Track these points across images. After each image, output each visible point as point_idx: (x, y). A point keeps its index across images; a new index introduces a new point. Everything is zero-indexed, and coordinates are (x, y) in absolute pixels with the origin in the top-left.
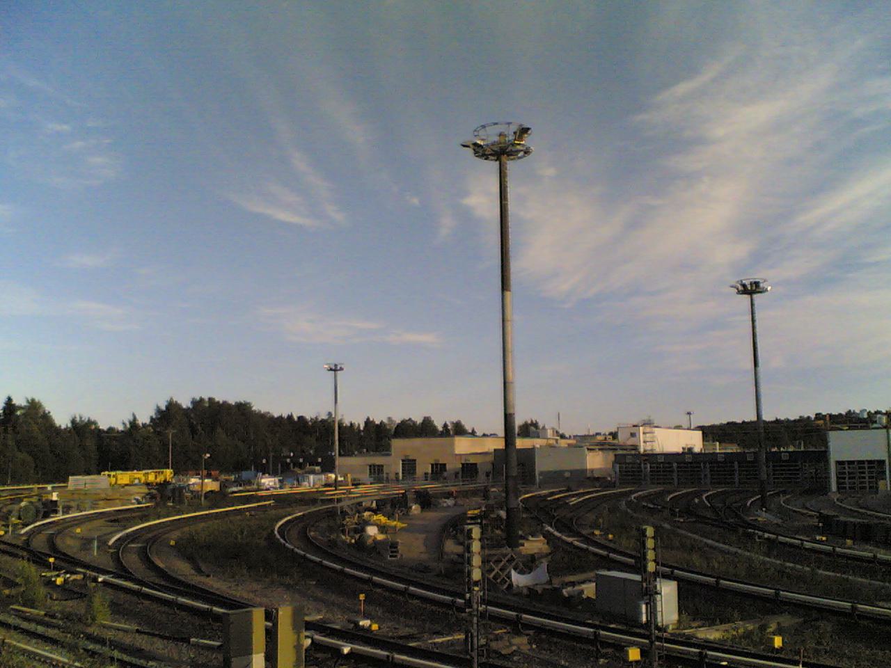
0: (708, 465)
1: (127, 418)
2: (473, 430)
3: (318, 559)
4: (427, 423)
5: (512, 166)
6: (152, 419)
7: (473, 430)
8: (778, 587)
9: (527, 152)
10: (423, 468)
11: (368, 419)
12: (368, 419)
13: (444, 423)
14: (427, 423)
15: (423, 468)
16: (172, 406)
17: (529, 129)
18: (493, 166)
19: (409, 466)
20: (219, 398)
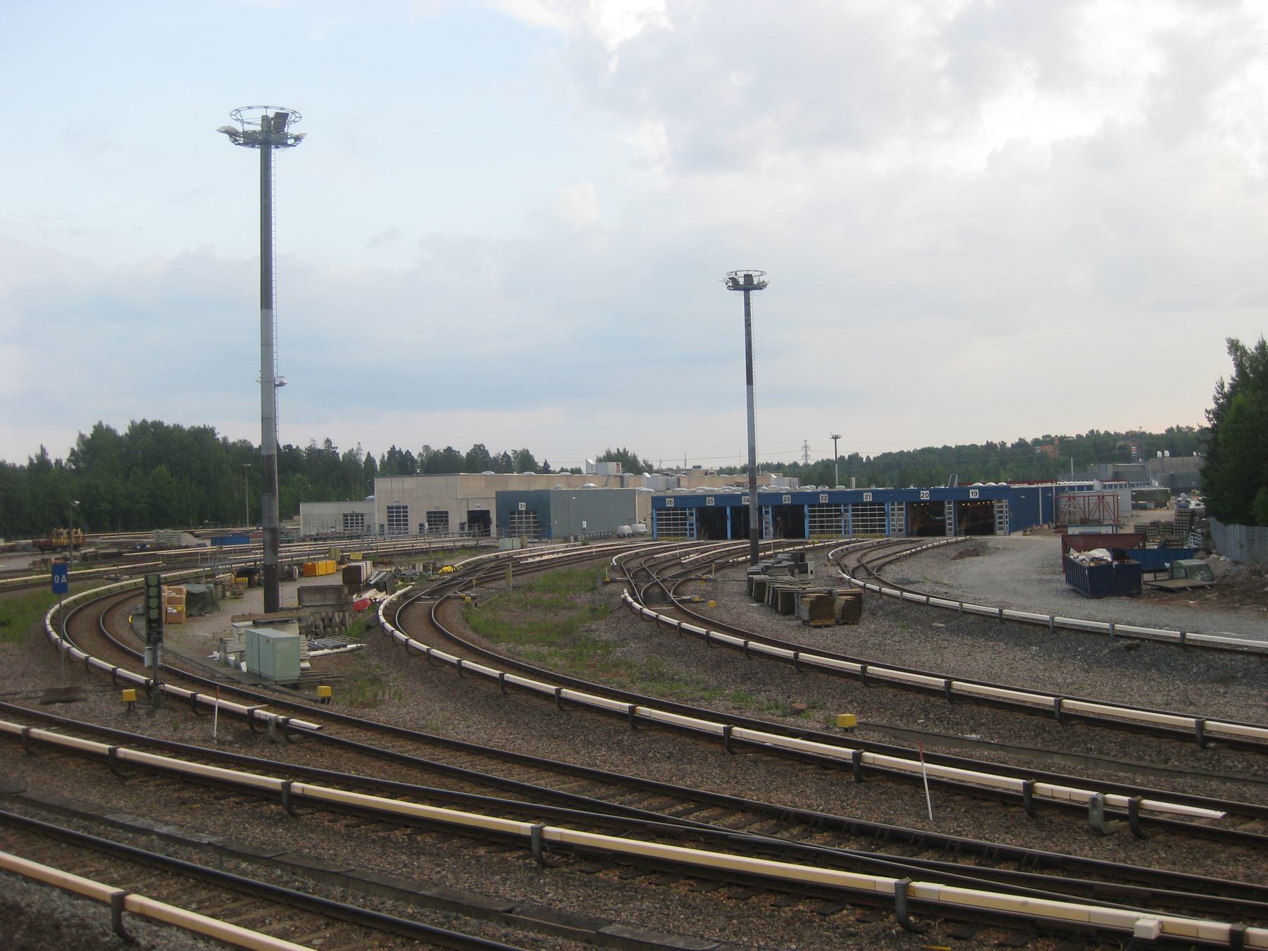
0: (850, 508)
1: (34, 452)
2: (546, 463)
3: (454, 659)
4: (479, 451)
5: (277, 154)
6: (73, 452)
7: (546, 463)
8: (1139, 781)
9: (298, 139)
10: (417, 518)
11: (393, 448)
12: (393, 448)
13: (77, 436)
14: (479, 451)
15: (417, 518)
16: (626, 453)
17: (282, 118)
18: (256, 152)
19: (398, 515)
20: (169, 422)
